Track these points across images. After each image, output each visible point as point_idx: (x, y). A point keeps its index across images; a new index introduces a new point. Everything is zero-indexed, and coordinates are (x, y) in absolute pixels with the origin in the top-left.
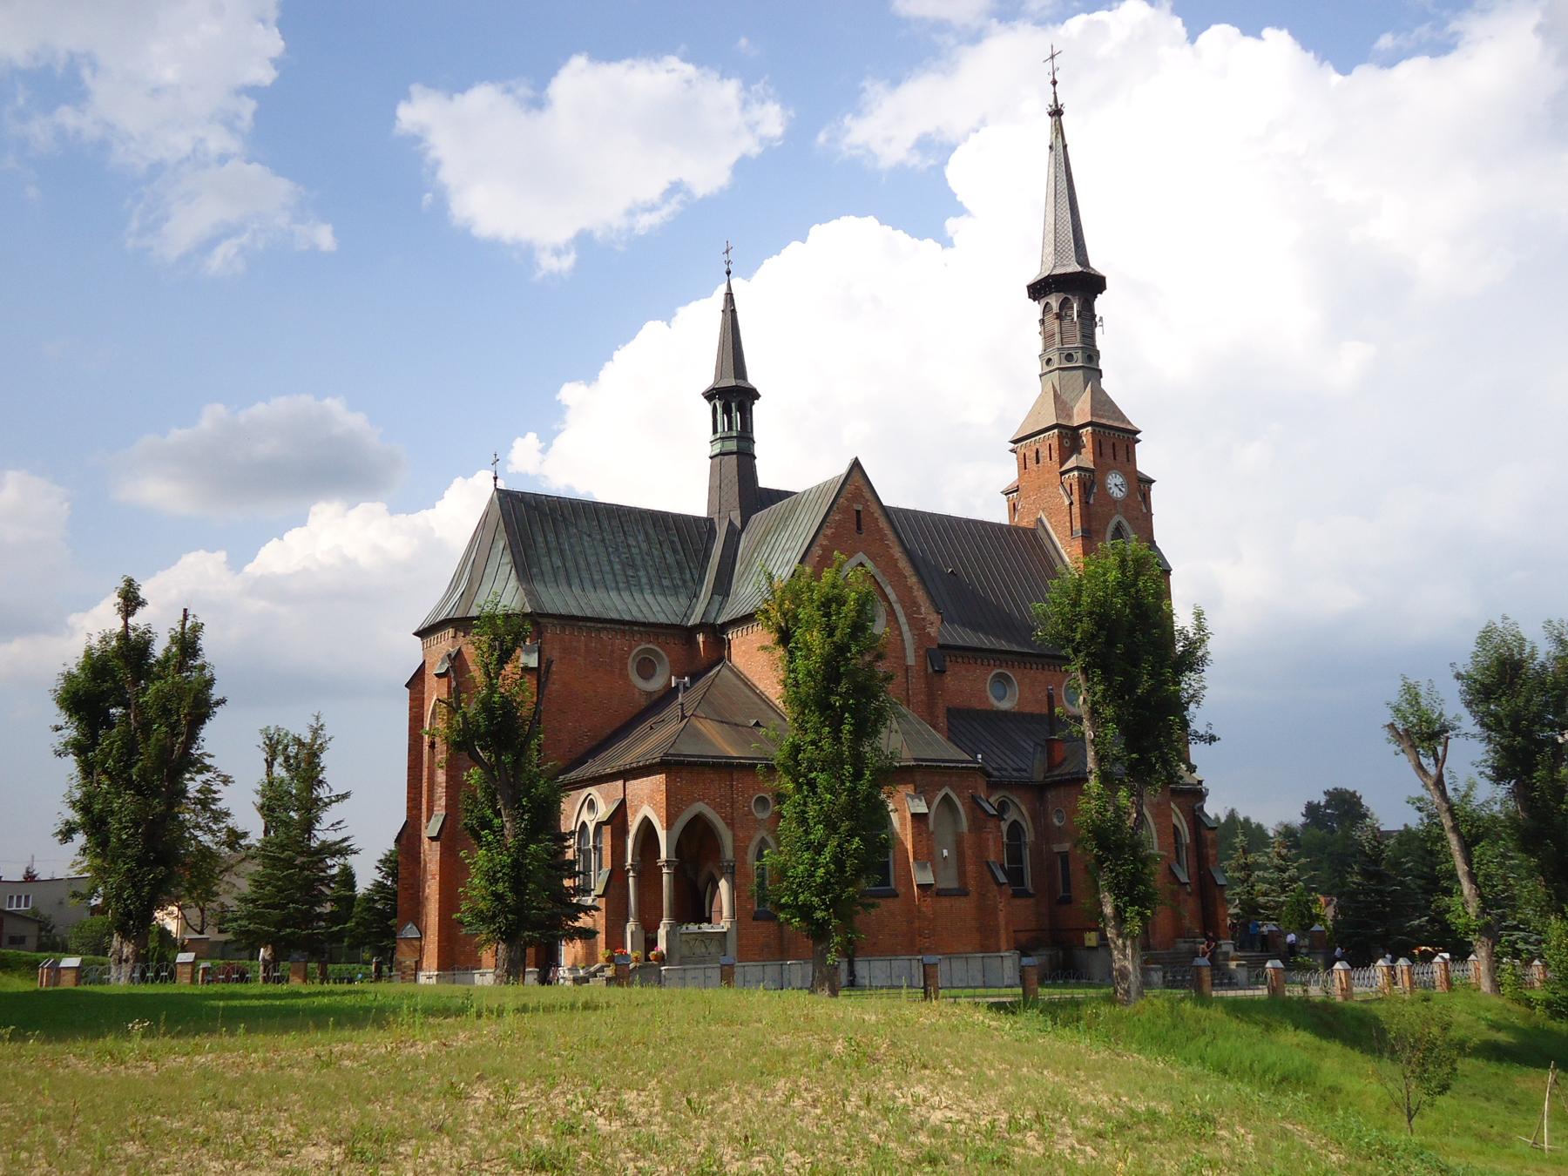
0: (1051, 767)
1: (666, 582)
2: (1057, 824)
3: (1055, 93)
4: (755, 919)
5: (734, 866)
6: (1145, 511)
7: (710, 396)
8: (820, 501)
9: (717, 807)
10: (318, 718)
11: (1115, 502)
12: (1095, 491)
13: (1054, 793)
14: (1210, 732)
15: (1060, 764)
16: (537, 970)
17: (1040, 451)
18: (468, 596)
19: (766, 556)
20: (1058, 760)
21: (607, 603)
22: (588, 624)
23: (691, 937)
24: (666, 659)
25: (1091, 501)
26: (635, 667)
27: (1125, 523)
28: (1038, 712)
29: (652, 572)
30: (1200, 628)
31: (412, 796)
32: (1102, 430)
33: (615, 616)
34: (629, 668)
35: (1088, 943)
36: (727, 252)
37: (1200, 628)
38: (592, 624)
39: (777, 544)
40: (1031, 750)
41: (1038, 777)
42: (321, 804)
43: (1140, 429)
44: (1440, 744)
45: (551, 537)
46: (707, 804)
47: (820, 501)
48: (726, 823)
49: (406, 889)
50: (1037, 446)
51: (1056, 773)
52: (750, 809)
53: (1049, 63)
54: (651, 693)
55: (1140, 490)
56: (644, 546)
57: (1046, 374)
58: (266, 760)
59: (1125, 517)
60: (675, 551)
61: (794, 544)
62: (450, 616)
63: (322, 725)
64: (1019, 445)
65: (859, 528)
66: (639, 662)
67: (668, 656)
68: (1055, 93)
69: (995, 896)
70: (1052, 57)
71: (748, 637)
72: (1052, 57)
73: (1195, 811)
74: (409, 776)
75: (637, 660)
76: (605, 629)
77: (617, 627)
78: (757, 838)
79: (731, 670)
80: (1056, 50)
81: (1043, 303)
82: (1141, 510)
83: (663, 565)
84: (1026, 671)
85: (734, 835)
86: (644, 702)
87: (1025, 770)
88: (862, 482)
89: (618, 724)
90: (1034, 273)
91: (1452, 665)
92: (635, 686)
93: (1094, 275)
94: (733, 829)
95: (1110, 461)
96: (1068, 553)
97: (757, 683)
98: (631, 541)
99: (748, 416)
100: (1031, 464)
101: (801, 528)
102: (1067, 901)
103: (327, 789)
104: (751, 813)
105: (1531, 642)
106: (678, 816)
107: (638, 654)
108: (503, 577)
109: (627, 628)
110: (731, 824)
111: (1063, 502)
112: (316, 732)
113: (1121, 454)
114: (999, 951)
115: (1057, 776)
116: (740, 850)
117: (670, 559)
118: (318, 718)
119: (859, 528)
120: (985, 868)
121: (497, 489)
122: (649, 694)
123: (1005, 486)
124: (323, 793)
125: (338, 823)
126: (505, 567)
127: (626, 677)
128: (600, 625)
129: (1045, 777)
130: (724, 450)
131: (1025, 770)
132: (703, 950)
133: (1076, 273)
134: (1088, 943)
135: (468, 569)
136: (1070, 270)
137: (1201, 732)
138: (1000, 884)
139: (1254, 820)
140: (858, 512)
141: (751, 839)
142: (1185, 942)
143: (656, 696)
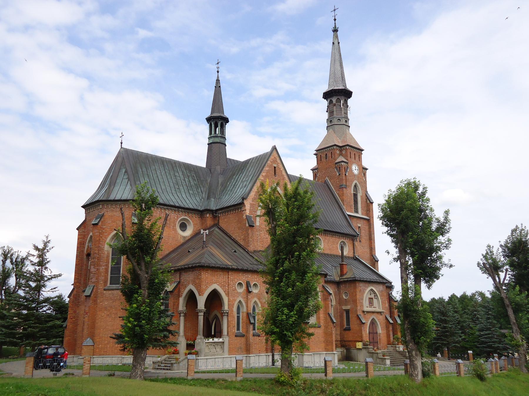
0: (342, 274)
1: (191, 192)
2: (345, 298)
3: (335, 23)
4: (236, 336)
5: (228, 313)
6: (364, 180)
7: (209, 120)
8: (258, 162)
9: (222, 286)
10: (47, 237)
11: (355, 175)
12: (348, 171)
13: (343, 286)
14: (450, 263)
15: (346, 274)
16: (133, 356)
17: (327, 155)
18: (109, 191)
19: (234, 183)
20: (345, 272)
21: (168, 198)
22: (161, 206)
23: (209, 343)
24: (192, 223)
25: (347, 174)
26: (179, 225)
27: (358, 183)
28: (330, 253)
29: (185, 187)
30: (446, 218)
31: (77, 277)
32: (351, 148)
33: (172, 204)
34: (177, 226)
35: (357, 347)
36: (218, 63)
37: (446, 218)
38: (163, 207)
39: (239, 179)
40: (331, 268)
41: (337, 279)
42: (46, 279)
43: (364, 149)
44: (503, 272)
45: (144, 169)
46: (218, 285)
47: (258, 162)
48: (226, 294)
49: (72, 319)
50: (326, 152)
51: (344, 277)
52: (235, 288)
53: (333, 13)
54: (185, 237)
55: (363, 172)
56: (182, 177)
57: (329, 126)
58: (2, 260)
59: (358, 182)
60: (194, 180)
61: (247, 179)
62: (101, 199)
63: (49, 241)
64: (319, 152)
65: (275, 174)
66: (180, 224)
67: (193, 222)
68: (335, 23)
69: (332, 328)
70: (335, 10)
71: (228, 216)
72: (335, 10)
73: (389, 294)
74: (76, 268)
75: (180, 223)
76: (168, 209)
77: (172, 208)
78: (238, 301)
79: (220, 229)
80: (336, 8)
81: (329, 100)
82: (363, 179)
83: (190, 185)
84: (326, 237)
85: (228, 299)
86: (182, 241)
87: (331, 276)
88: (277, 155)
89: (171, 250)
90: (326, 88)
91: (500, 242)
92: (179, 234)
93: (347, 90)
94: (228, 296)
95: (353, 160)
96: (337, 193)
97: (232, 235)
98: (177, 174)
99: (224, 129)
100: (324, 160)
101: (250, 173)
102: (348, 329)
103: (49, 272)
104: (236, 290)
105: (449, 240)
106: (206, 290)
107: (179, 222)
108: (124, 184)
109: (177, 209)
110: (228, 294)
111: (336, 174)
112: (46, 244)
113: (357, 158)
114: (333, 351)
115: (346, 278)
116: (230, 306)
117: (192, 183)
118: (47, 237)
119: (275, 174)
120: (328, 316)
121: (121, 148)
122: (184, 237)
123: (312, 168)
124: (46, 273)
125: (55, 288)
126: (125, 180)
127: (175, 230)
128: (166, 207)
129: (340, 279)
130: (214, 141)
131: (331, 276)
132: (214, 350)
133: (342, 89)
134: (357, 347)
135: (109, 179)
136: (340, 88)
137: (446, 263)
138: (333, 323)
139: (437, 298)
140: (275, 167)
141: (235, 300)
142: (392, 347)
143: (187, 239)
